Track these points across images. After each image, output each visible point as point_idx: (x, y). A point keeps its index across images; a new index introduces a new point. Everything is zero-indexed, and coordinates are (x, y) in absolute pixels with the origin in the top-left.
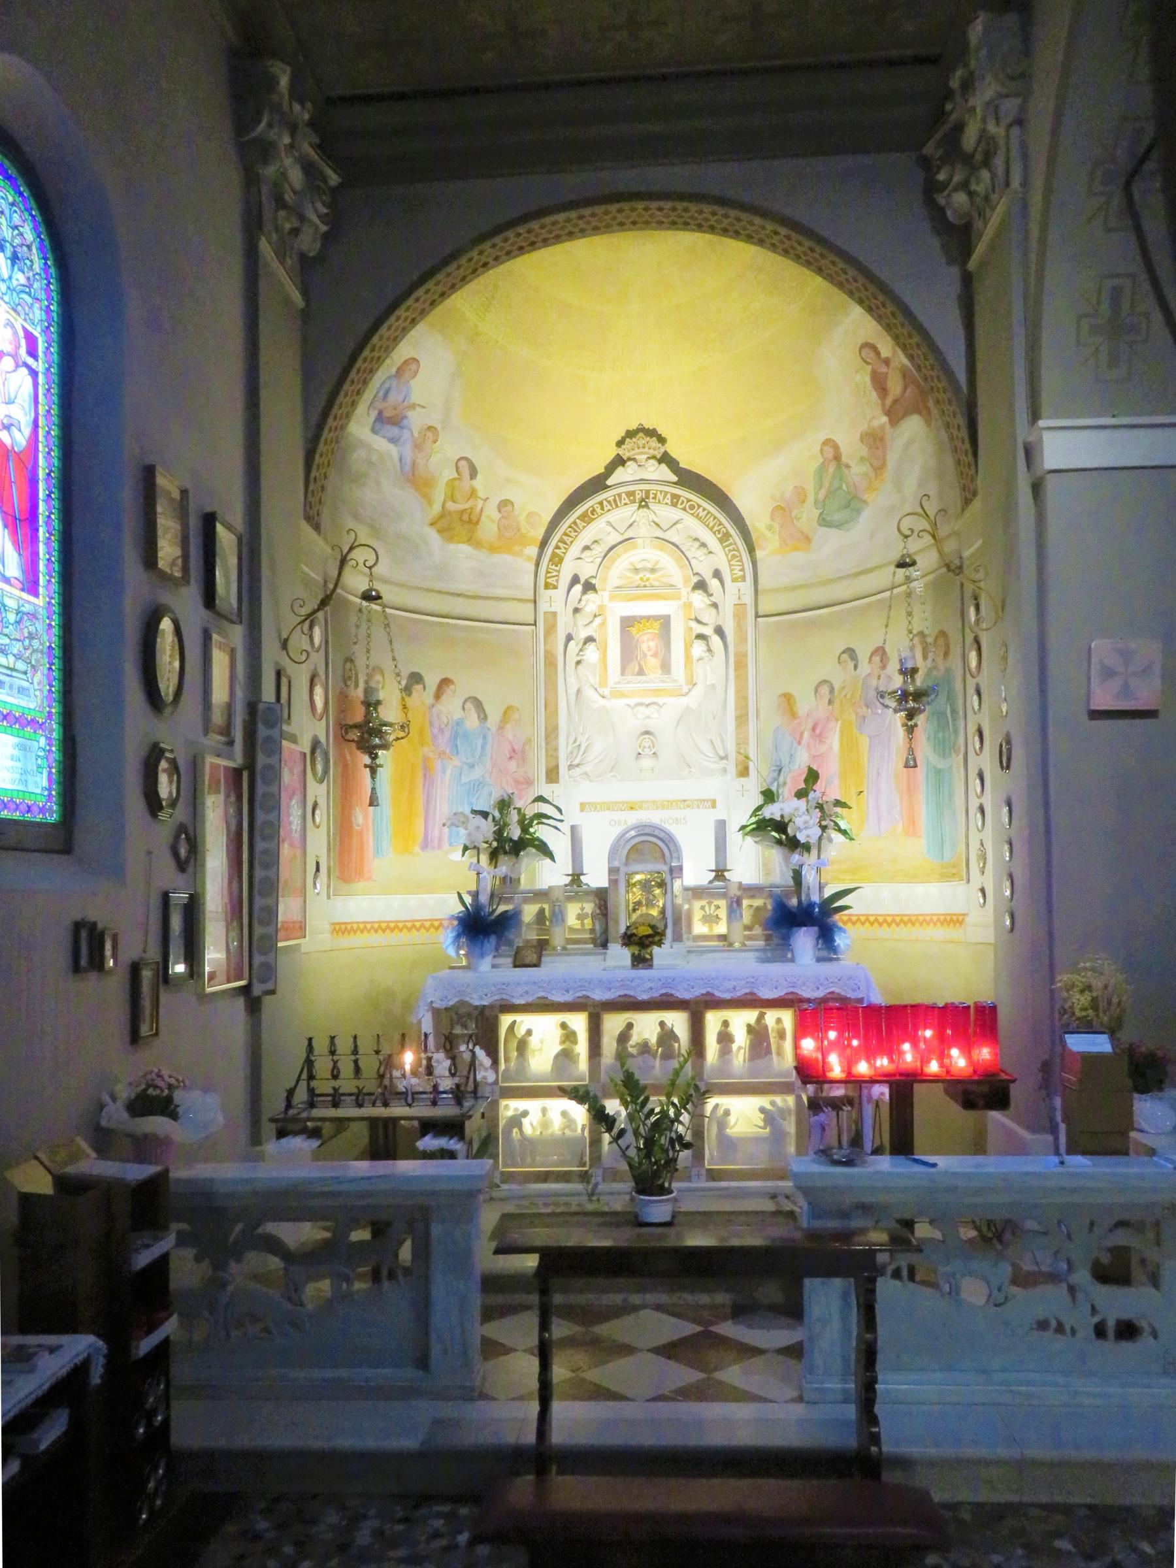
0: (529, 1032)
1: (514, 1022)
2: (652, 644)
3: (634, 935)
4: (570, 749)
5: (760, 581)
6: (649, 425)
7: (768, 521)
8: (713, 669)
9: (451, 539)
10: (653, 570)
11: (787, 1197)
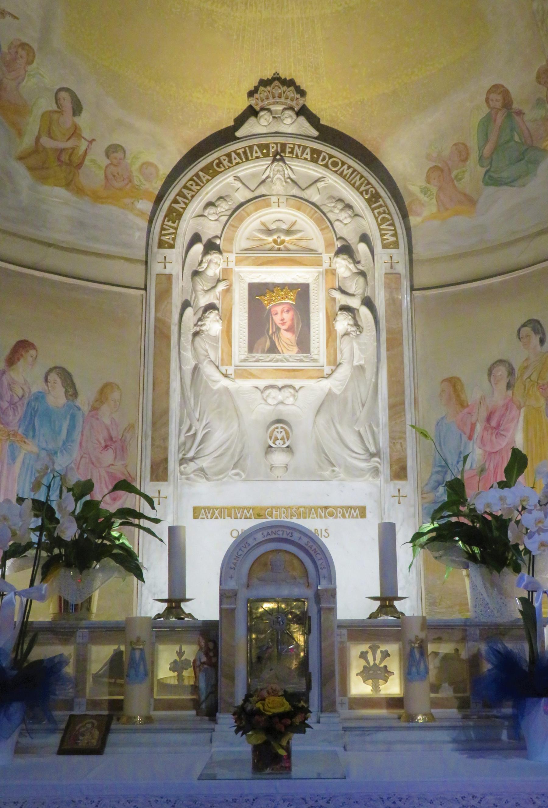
2: (287, 317)
3: (258, 712)
4: (182, 438)
5: (415, 251)
6: (285, 74)
7: (424, 184)
8: (361, 348)
9: (44, 180)
10: (288, 232)
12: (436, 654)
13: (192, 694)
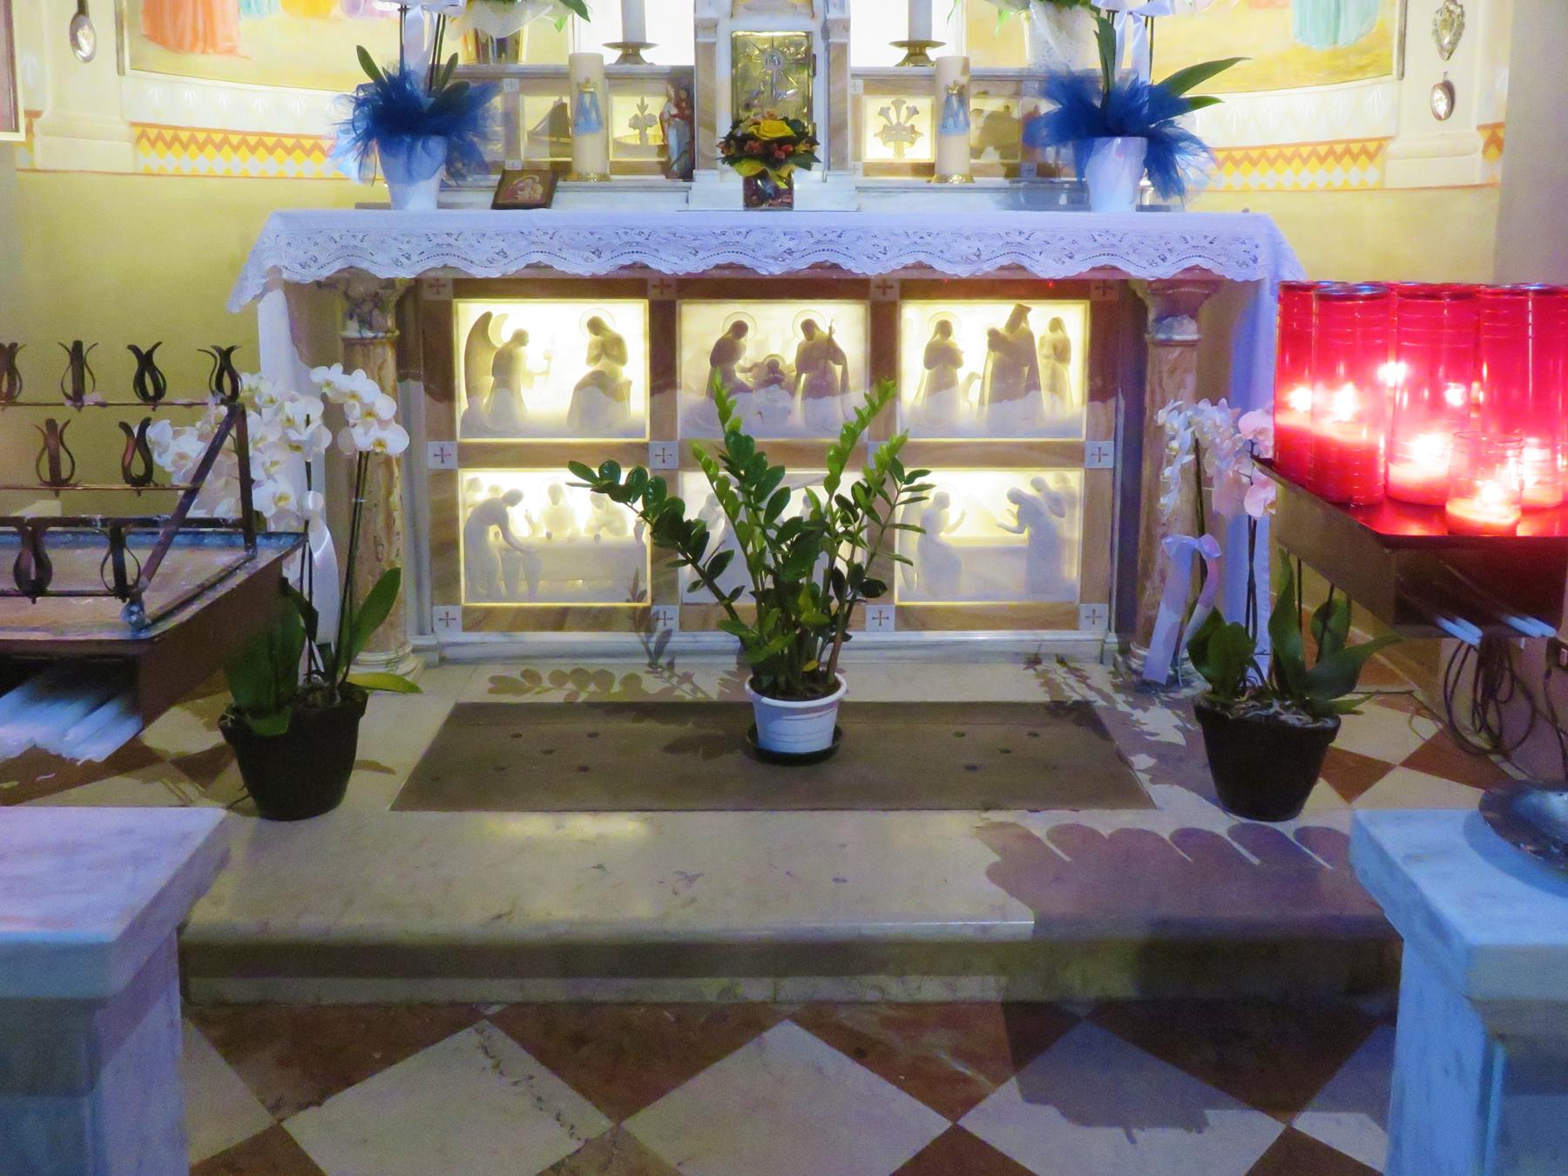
0: (520, 338)
1: (486, 318)
11: (1061, 661)
12: (979, 111)
13: (659, 155)
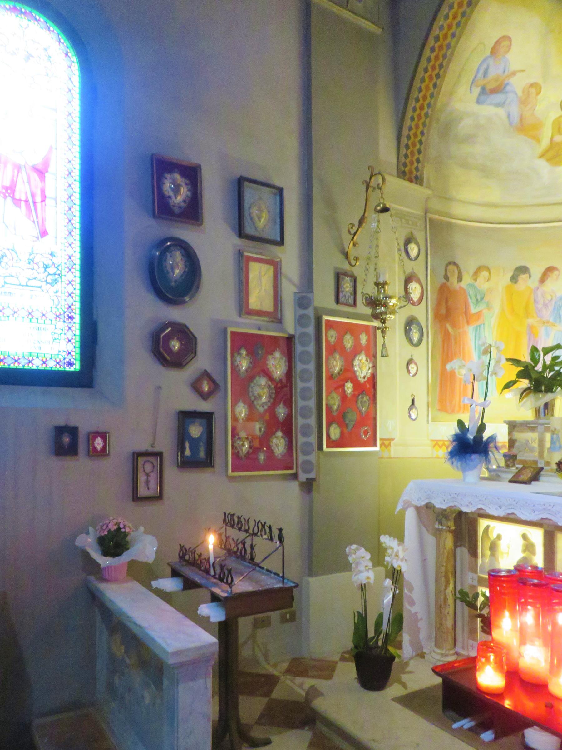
0: (499, 537)
